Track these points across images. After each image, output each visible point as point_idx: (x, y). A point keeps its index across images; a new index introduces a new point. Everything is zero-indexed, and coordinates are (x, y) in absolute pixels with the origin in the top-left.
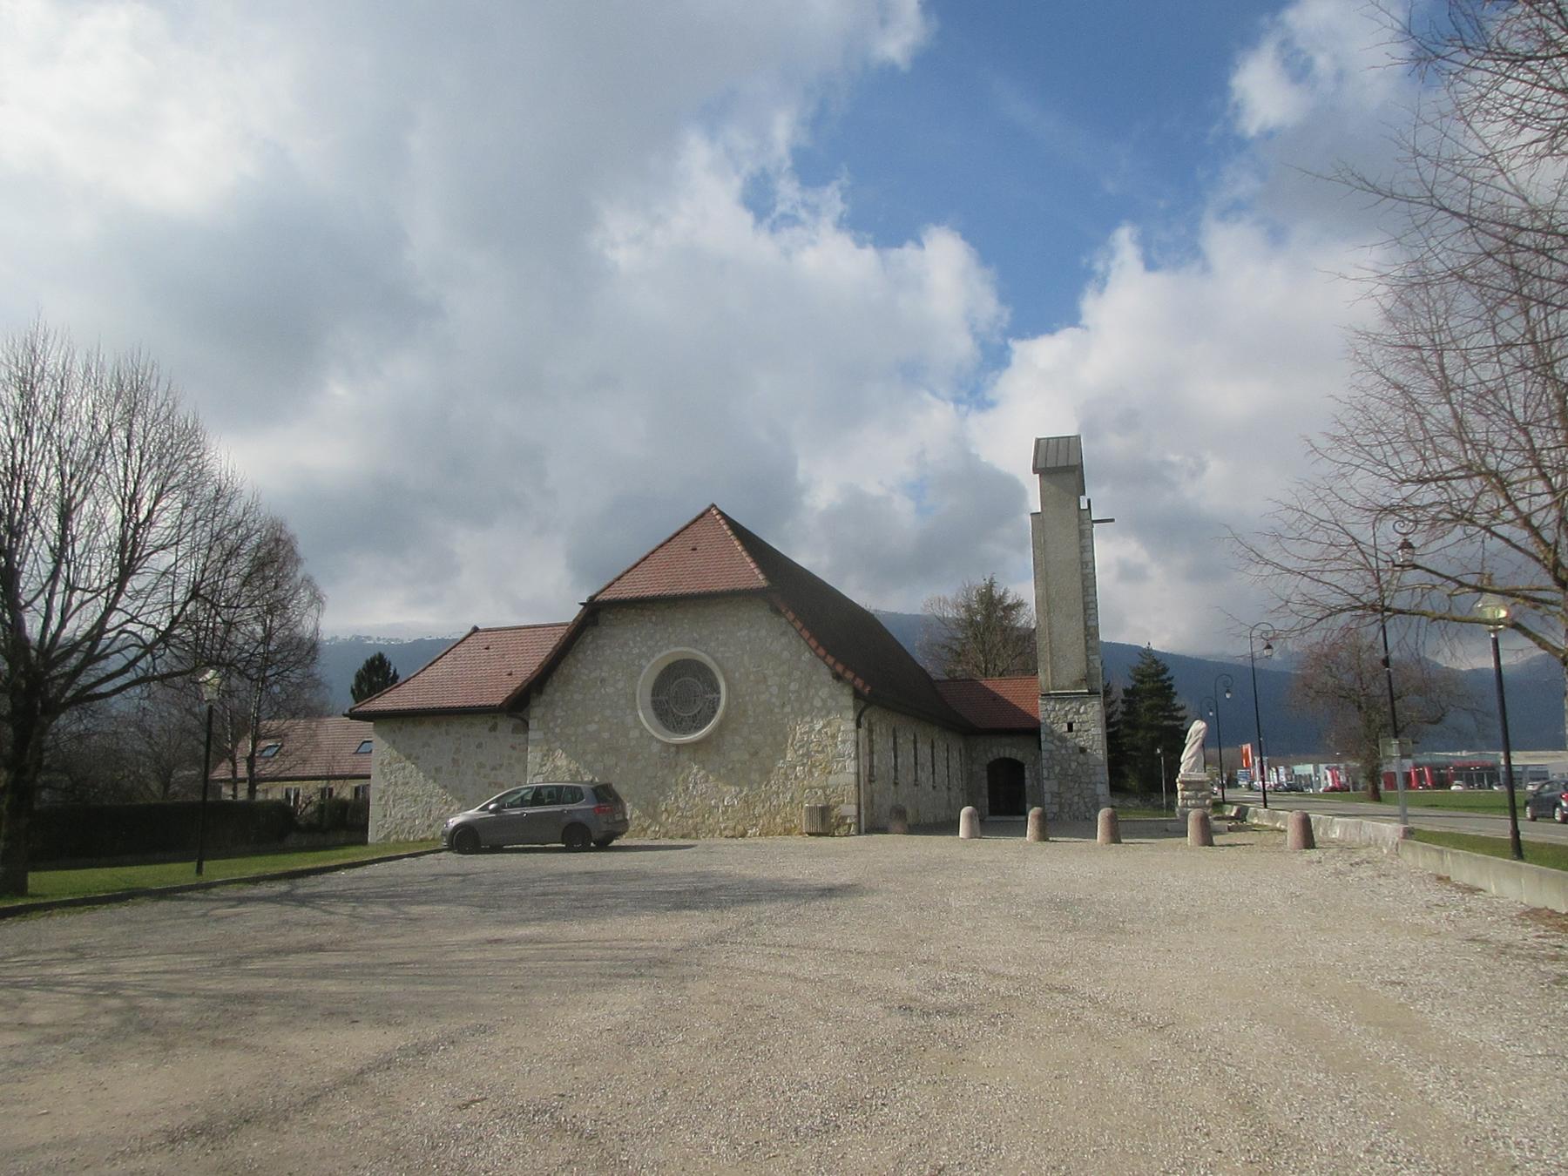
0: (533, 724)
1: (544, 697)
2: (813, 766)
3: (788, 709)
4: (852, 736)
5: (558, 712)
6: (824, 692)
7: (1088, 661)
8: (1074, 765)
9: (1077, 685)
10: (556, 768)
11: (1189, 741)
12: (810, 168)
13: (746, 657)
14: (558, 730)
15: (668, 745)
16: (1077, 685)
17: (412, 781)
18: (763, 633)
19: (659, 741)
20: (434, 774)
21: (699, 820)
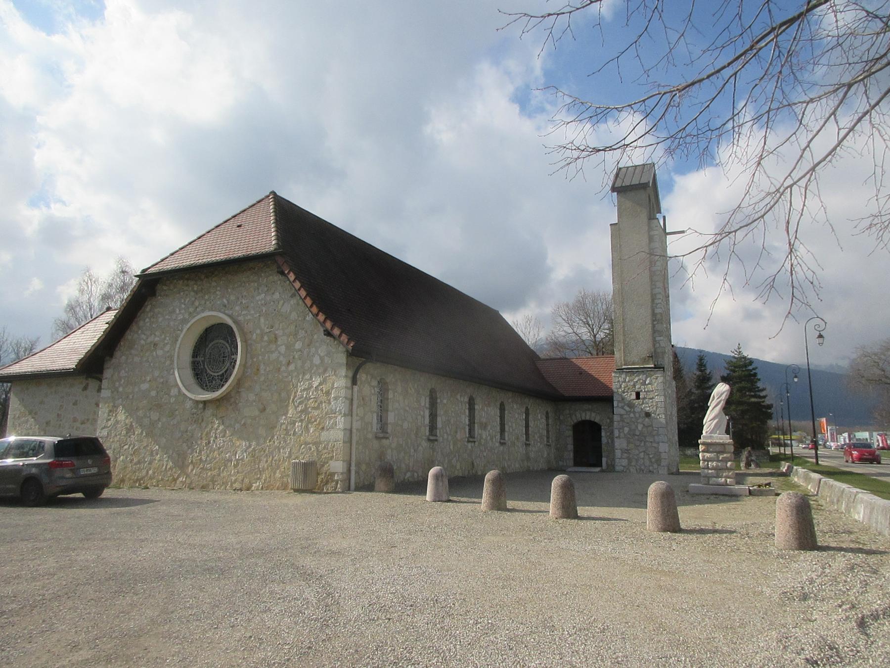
0: (105, 383)
1: (114, 360)
2: (309, 422)
3: (292, 367)
4: (343, 393)
5: (123, 373)
6: (322, 351)
7: (654, 341)
8: (640, 427)
9: (645, 361)
10: (117, 422)
11: (712, 404)
12: (551, 85)
13: (262, 320)
14: (121, 389)
15: (197, 402)
16: (645, 361)
19: (191, 399)
21: (215, 472)
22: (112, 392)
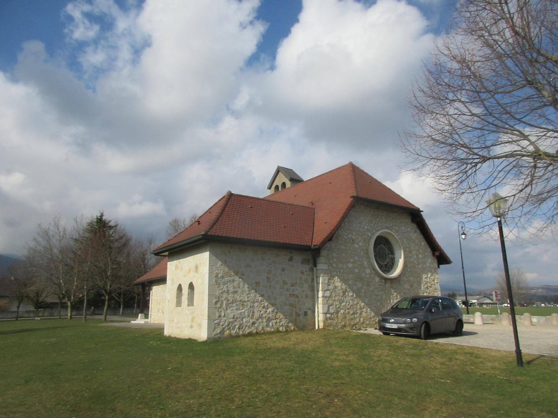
10: (336, 287)
14: (334, 265)
17: (240, 291)
18: (409, 230)
20: (255, 286)
22: (329, 266)
